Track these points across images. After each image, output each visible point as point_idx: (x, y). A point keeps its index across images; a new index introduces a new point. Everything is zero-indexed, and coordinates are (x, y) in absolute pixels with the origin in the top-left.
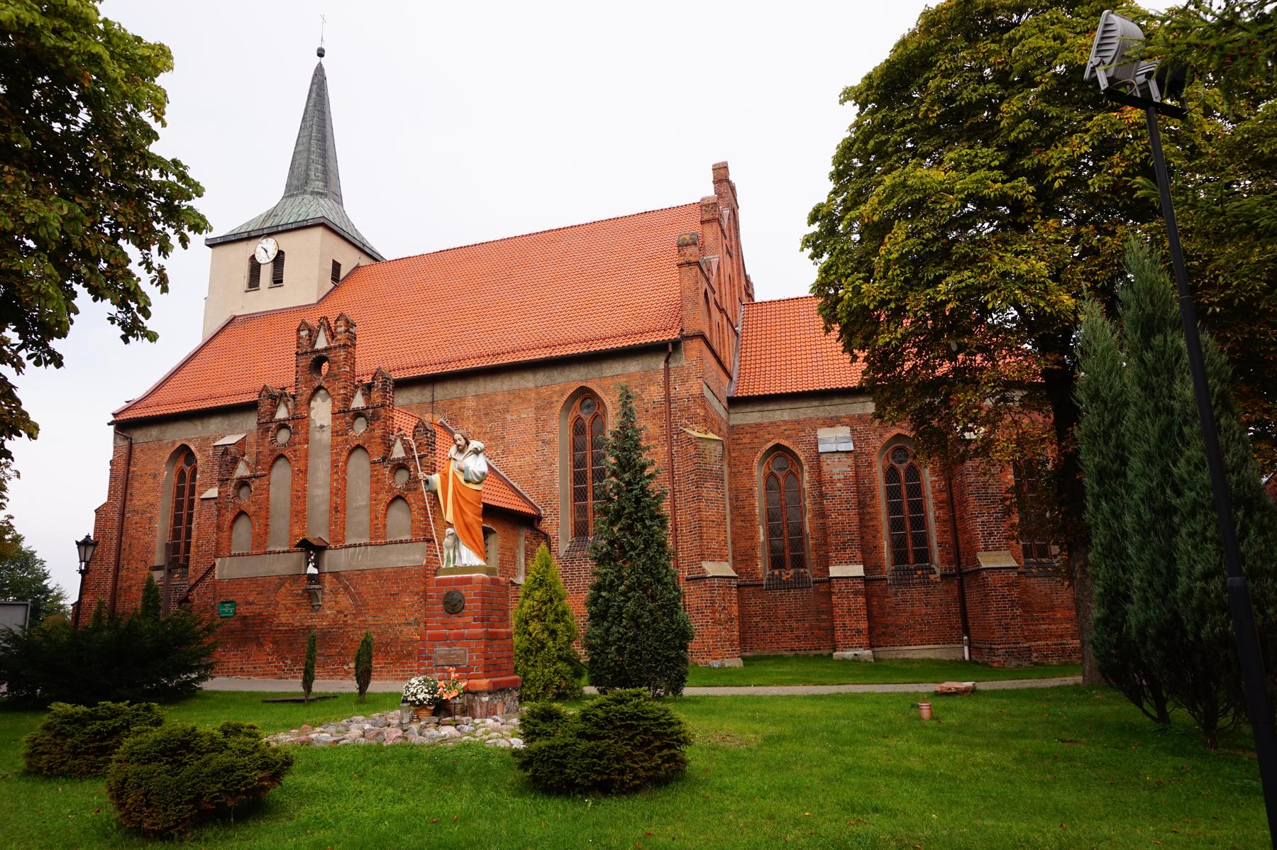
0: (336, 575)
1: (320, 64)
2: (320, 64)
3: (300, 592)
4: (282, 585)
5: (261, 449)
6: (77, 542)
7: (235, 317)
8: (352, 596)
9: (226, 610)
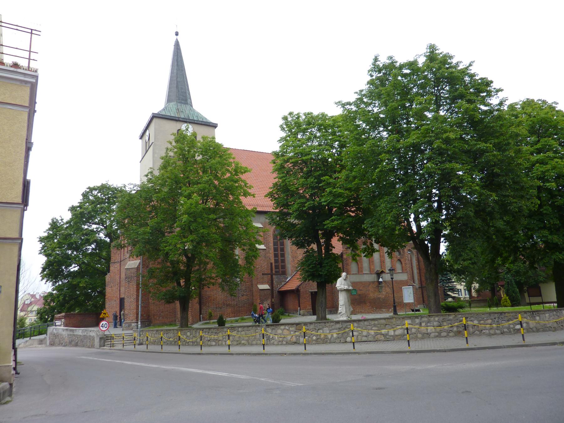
0: (385, 282)
1: (177, 39)
2: (177, 39)
6: (432, 48)
9: (353, 292)
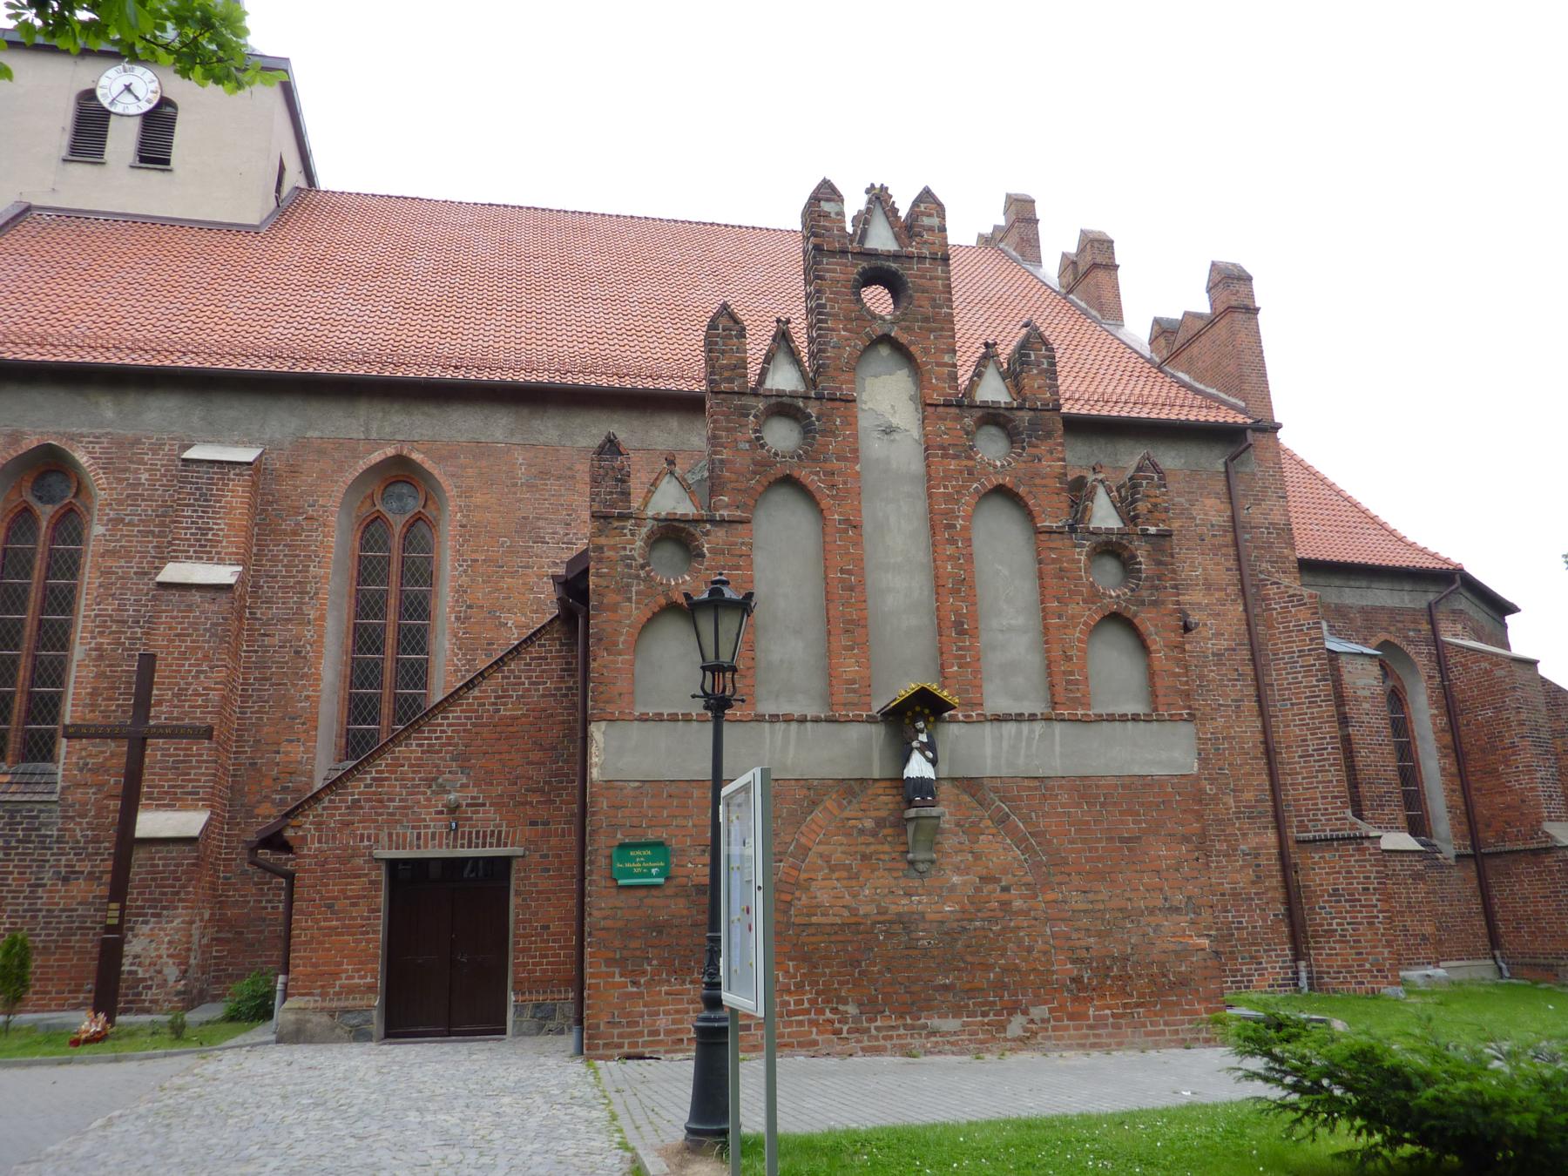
0: (970, 785)
3: (869, 824)
4: (814, 803)
5: (725, 454)
7: (29, 208)
8: (1021, 841)
9: (636, 867)
